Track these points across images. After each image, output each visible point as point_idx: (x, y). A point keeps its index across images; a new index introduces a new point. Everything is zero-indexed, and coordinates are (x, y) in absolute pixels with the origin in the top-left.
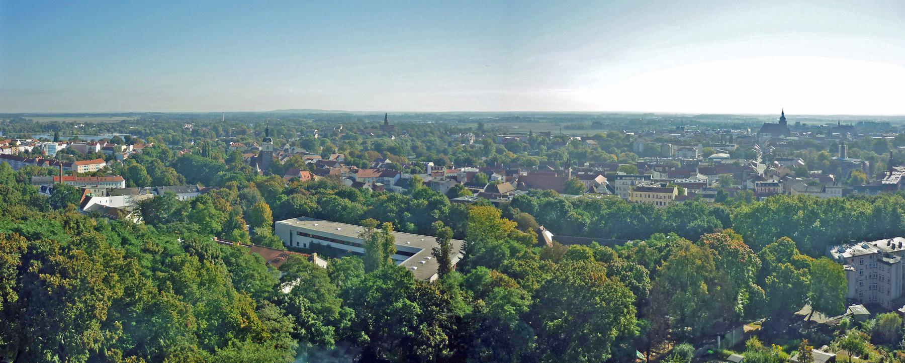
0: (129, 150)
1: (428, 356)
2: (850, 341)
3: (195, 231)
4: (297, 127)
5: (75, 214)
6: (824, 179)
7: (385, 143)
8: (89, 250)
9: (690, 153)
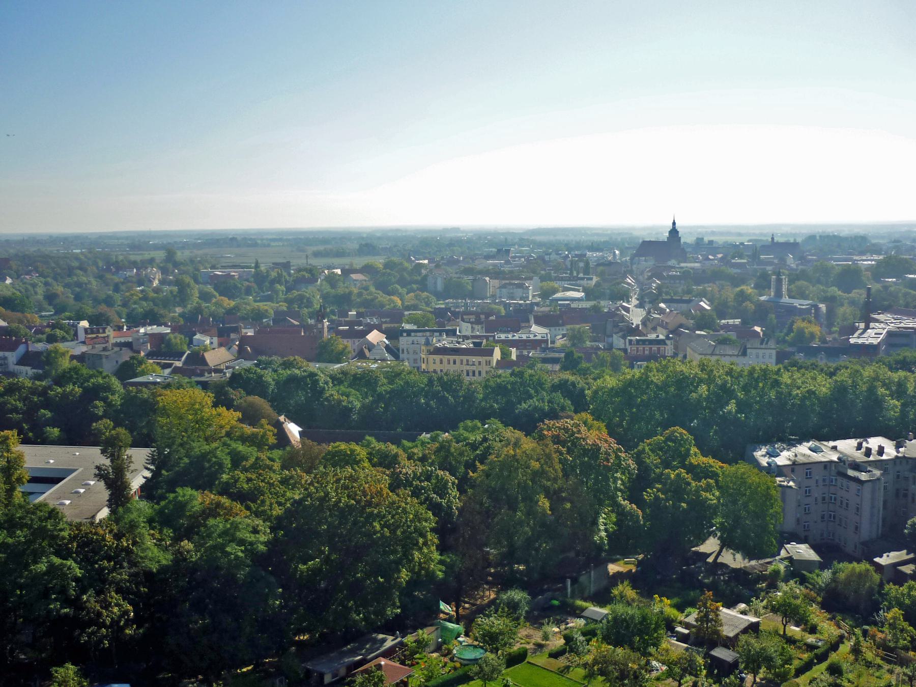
1: (101, 641)
2: (785, 601)
6: (745, 332)
9: (519, 292)
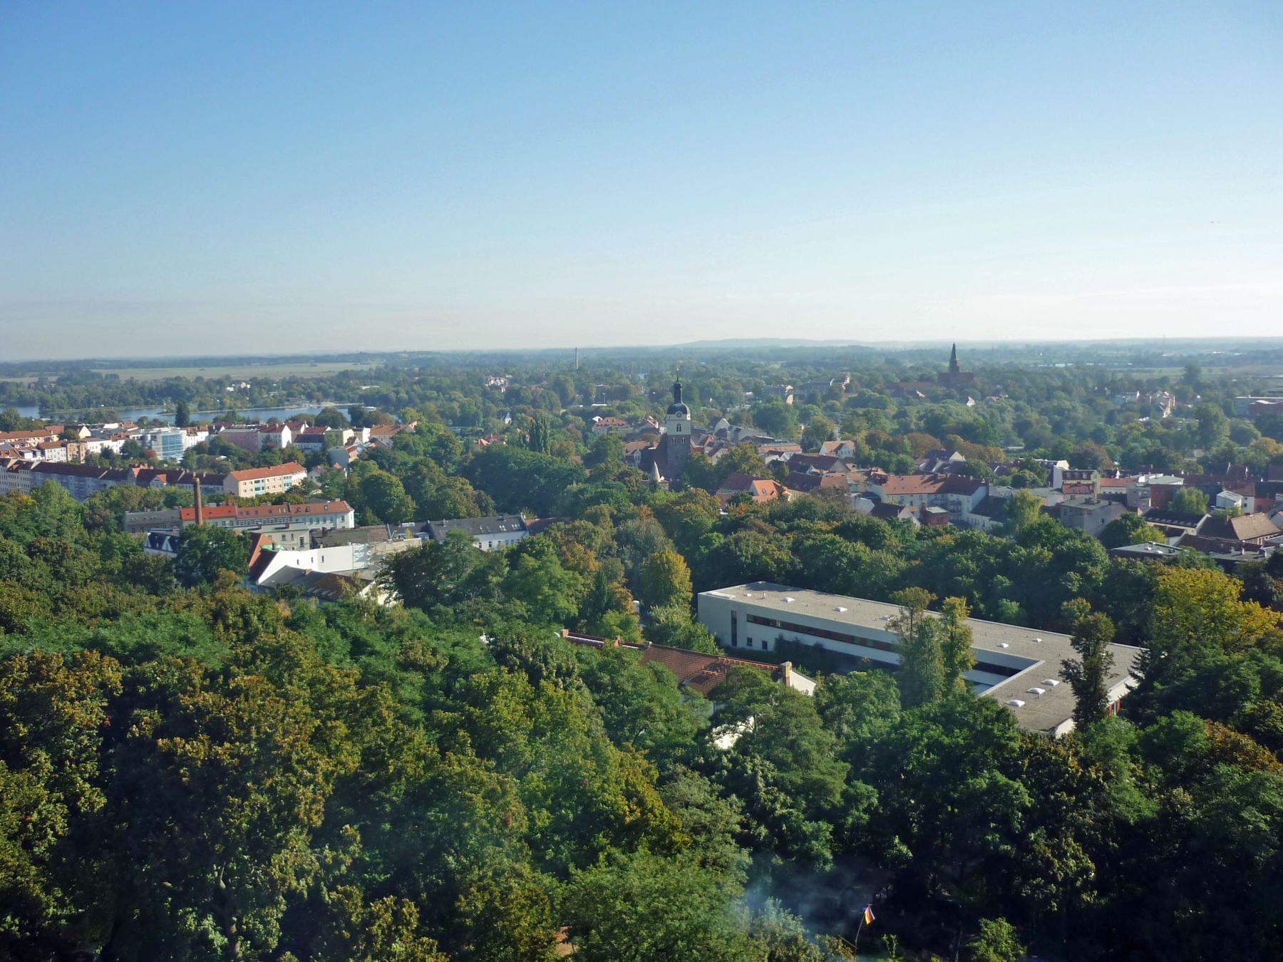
0: (361, 438)
3: (517, 618)
4: (744, 380)
5: (237, 594)
7: (950, 415)
8: (275, 673)
